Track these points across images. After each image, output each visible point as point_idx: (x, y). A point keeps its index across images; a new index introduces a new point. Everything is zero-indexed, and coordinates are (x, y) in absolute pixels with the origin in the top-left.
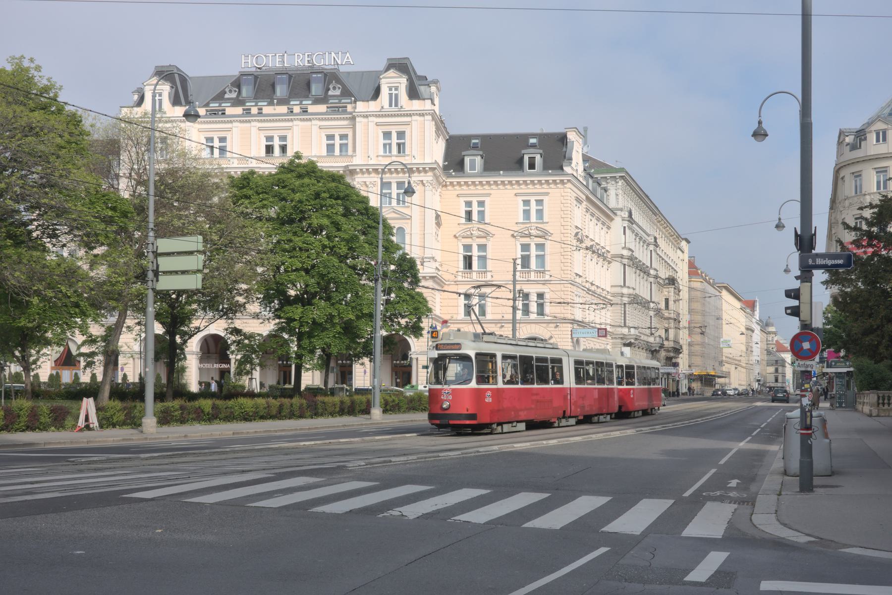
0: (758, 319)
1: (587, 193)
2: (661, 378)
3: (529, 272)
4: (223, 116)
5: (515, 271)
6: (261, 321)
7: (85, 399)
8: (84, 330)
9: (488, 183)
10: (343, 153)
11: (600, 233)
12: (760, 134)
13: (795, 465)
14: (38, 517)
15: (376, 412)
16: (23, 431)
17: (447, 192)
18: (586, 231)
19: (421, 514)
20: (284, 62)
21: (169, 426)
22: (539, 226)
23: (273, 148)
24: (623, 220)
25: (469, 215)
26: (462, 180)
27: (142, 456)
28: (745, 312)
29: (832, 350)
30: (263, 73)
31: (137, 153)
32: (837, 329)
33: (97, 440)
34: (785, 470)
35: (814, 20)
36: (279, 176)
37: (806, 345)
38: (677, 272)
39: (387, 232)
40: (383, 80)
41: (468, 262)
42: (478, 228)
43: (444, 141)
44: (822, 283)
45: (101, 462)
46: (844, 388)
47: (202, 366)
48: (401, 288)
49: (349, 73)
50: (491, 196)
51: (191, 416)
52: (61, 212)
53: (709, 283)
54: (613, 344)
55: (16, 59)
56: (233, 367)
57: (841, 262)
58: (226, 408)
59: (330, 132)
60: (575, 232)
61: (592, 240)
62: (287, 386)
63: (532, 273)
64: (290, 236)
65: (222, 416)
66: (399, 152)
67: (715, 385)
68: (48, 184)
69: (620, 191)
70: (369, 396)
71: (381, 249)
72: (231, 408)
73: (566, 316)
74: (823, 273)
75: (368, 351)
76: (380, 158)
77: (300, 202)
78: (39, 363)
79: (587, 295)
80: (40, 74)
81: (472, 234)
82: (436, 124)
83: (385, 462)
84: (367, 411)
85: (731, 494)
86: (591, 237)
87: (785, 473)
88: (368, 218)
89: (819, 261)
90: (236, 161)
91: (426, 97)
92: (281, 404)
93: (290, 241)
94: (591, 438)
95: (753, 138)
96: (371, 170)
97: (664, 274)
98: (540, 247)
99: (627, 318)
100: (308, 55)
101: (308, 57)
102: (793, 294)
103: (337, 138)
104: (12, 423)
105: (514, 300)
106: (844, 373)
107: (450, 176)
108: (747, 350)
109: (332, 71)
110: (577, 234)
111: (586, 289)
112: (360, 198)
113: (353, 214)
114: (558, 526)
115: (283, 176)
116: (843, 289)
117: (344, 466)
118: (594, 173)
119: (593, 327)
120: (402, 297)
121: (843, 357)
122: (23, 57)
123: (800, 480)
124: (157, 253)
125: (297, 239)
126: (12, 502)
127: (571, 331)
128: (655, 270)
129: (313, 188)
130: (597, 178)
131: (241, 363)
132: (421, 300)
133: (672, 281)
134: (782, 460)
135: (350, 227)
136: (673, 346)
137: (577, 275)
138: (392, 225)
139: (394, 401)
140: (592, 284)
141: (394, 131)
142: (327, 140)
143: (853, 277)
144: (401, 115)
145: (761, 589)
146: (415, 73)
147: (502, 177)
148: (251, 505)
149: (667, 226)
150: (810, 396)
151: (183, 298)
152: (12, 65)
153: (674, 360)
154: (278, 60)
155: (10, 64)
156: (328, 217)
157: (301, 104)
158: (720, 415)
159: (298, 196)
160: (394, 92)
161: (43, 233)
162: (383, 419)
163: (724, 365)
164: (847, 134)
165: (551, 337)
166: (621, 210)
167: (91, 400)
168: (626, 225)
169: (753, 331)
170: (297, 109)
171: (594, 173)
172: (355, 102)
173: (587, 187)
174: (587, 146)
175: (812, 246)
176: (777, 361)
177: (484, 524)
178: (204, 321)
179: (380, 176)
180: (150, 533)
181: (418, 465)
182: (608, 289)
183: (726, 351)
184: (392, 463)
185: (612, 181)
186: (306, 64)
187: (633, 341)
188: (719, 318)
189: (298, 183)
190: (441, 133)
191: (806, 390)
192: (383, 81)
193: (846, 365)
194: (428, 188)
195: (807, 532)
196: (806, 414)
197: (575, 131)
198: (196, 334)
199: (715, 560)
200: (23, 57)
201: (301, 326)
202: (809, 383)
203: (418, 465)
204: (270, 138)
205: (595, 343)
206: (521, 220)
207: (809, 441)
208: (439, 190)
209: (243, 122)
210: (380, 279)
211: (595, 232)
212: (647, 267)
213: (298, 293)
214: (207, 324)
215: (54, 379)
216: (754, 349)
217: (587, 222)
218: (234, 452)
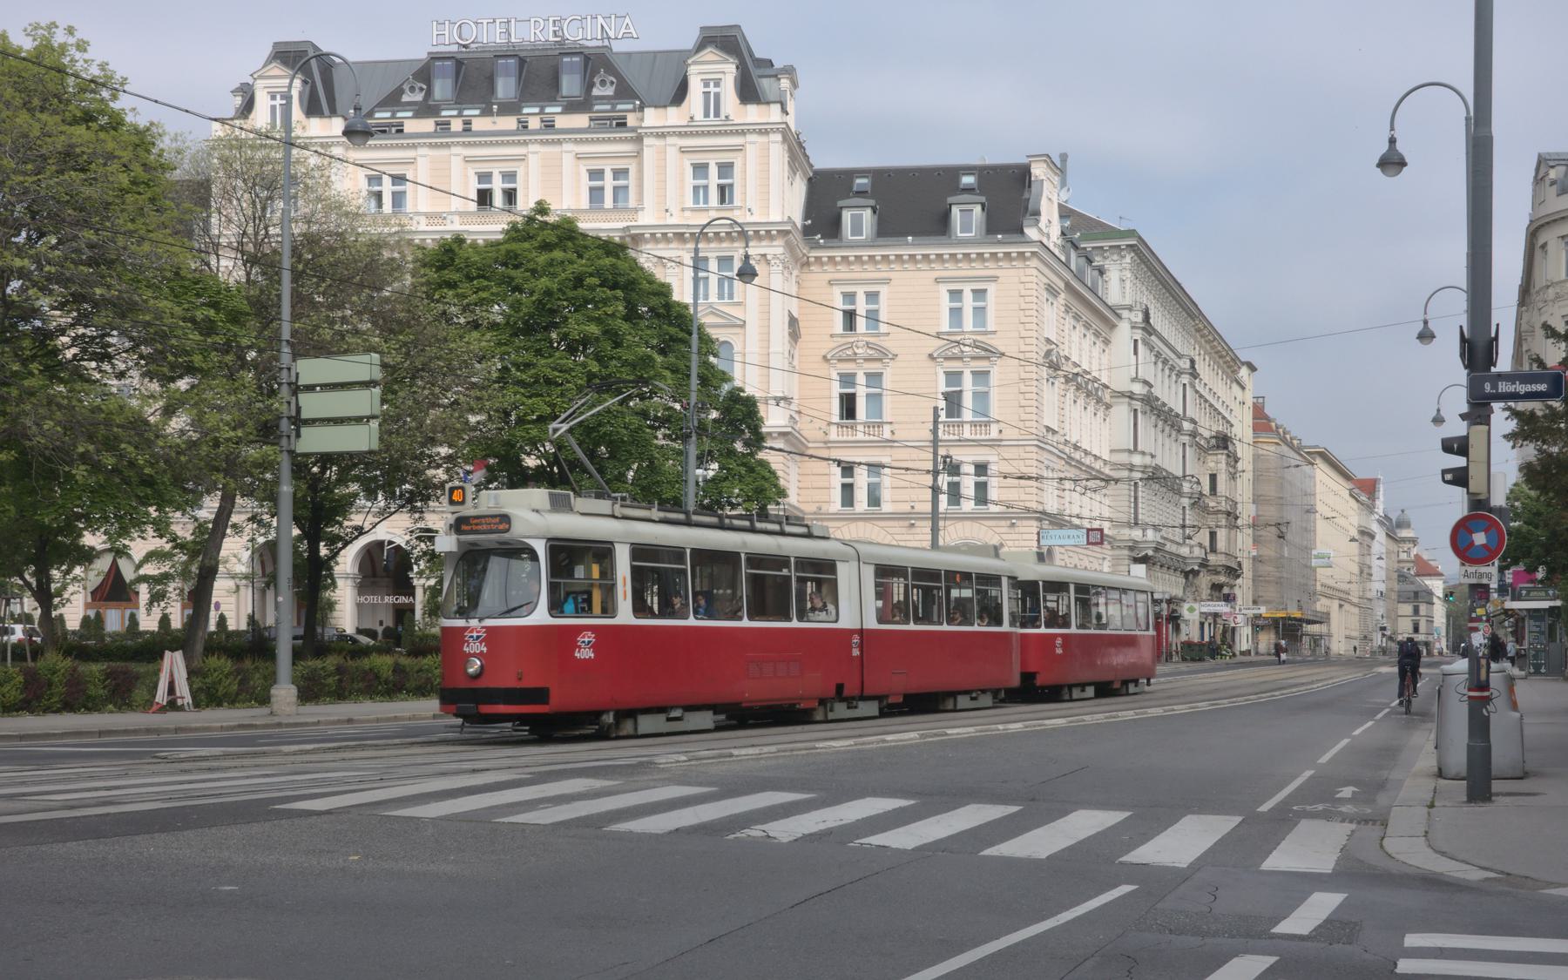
0: (1382, 514)
1: (1068, 277)
4: (399, 135)
5: (936, 422)
7: (168, 654)
8: (162, 529)
9: (885, 258)
10: (620, 205)
12: (1392, 162)
13: (1458, 759)
14: (137, 838)
16: (58, 711)
18: (1066, 347)
20: (510, 35)
21: (317, 704)
22: (979, 338)
23: (491, 194)
24: (1133, 328)
26: (838, 254)
27: (286, 748)
28: (1358, 501)
29: (1521, 567)
30: (471, 56)
31: (254, 202)
32: (1530, 527)
34: (1440, 769)
36: (507, 246)
37: (1480, 538)
38: (1232, 426)
39: (704, 350)
41: (848, 406)
42: (867, 343)
45: (216, 758)
46: (1543, 639)
47: (362, 599)
48: (731, 453)
49: (629, 54)
52: (124, 309)
53: (1291, 446)
54: (1115, 559)
55: (42, 28)
58: (418, 672)
59: (596, 165)
60: (1045, 349)
61: (1076, 365)
63: (967, 427)
64: (527, 356)
65: (411, 684)
66: (722, 200)
67: (1301, 637)
69: (1129, 275)
71: (694, 382)
72: (427, 670)
73: (1028, 505)
74: (1507, 419)
76: (687, 214)
77: (548, 293)
78: (66, 596)
79: (1067, 467)
80: (86, 56)
81: (856, 354)
82: (791, 150)
83: (720, 756)
85: (1343, 809)
86: (1074, 358)
87: (1440, 774)
88: (671, 324)
89: (1504, 387)
90: (423, 220)
91: (772, 99)
93: (528, 365)
94: (1084, 721)
95: (1407, 161)
96: (670, 235)
97: (1208, 428)
98: (980, 376)
99: (1140, 511)
100: (554, 21)
101: (554, 26)
103: (608, 175)
104: (38, 698)
105: (936, 473)
106: (1544, 610)
108: (1362, 572)
109: (598, 51)
110: (1048, 353)
111: (1065, 457)
112: (655, 286)
115: (514, 246)
117: (651, 763)
119: (1077, 527)
120: (732, 469)
121: (1541, 582)
122: (54, 25)
124: (298, 387)
125: (543, 361)
127: (1038, 534)
128: (1193, 421)
129: (570, 268)
130: (1085, 248)
132: (767, 475)
133: (1223, 442)
134: (1435, 751)
136: (1224, 563)
137: (1048, 429)
138: (714, 337)
140: (1076, 447)
141: (712, 162)
143: (1562, 425)
144: (726, 133)
145: (1406, 945)
146: (751, 54)
147: (910, 247)
148: (506, 820)
149: (1215, 339)
150: (1486, 629)
151: (332, 473)
152: (35, 40)
153: (1226, 590)
154: (498, 31)
155: (31, 38)
156: (598, 320)
157: (542, 112)
158: (1315, 686)
159: (544, 282)
160: (712, 89)
161: (84, 350)
163: (1318, 600)
164: (1552, 163)
166: (1130, 309)
167: (178, 656)
168: (1138, 337)
169: (1372, 537)
170: (534, 123)
171: (1080, 239)
172: (641, 109)
173: (1067, 265)
174: (1066, 189)
175: (1491, 360)
176: (1416, 594)
178: (370, 516)
180: (340, 860)
182: (1106, 457)
183: (1323, 575)
184: (734, 758)
185: (1113, 254)
187: (1150, 553)
188: (1311, 510)
189: (542, 259)
191: (1479, 619)
192: (693, 70)
193: (1548, 595)
194: (775, 268)
195: (1484, 864)
196: (1479, 662)
197: (1045, 161)
198: (356, 538)
199: (1319, 907)
200: (54, 25)
202: (1484, 606)
204: (484, 177)
205: (1081, 557)
206: (945, 327)
207: (1484, 710)
209: (436, 146)
210: (694, 435)
211: (1081, 350)
212: (1177, 415)
213: (545, 463)
215: (92, 625)
216: (1375, 571)
217: (1067, 331)
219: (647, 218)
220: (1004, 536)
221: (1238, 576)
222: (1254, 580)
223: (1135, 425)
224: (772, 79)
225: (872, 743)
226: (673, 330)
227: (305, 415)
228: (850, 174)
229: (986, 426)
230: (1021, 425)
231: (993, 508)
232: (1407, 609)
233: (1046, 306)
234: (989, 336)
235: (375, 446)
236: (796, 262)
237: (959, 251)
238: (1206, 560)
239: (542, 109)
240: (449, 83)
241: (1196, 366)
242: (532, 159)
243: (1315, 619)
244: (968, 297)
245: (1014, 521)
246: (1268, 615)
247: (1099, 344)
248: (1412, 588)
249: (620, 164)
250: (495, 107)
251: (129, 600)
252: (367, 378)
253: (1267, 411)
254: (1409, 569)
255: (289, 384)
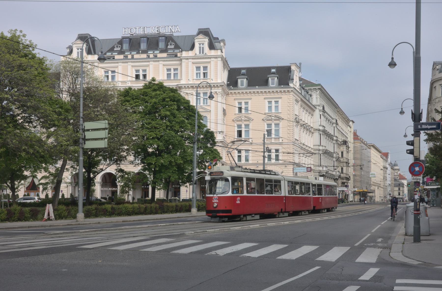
0: (390, 162)
1: (302, 97)
2: (339, 194)
3: (271, 138)
5: (264, 138)
6: (134, 165)
7: (48, 205)
10: (176, 78)
11: (308, 118)
12: (392, 64)
13: (411, 230)
15: (194, 210)
16: (17, 221)
17: (229, 98)
19: (226, 254)
20: (145, 31)
24: (320, 111)
25: (240, 109)
26: (237, 91)
28: (383, 159)
29: (429, 177)
32: (431, 166)
33: (55, 225)
35: (422, 5)
36: (144, 90)
37: (417, 169)
38: (347, 138)
40: (196, 40)
42: (245, 116)
43: (228, 71)
44: (424, 140)
46: (435, 197)
47: (103, 189)
48: (207, 147)
49: (178, 36)
50: (252, 99)
51: (101, 213)
52: (36, 109)
53: (364, 144)
55: (13, 31)
56: (119, 188)
57: (435, 127)
58: (118, 209)
59: (169, 67)
60: (295, 117)
62: (147, 198)
63: (273, 139)
64: (149, 121)
66: (204, 77)
68: (29, 95)
69: (318, 96)
70: (190, 203)
71: (196, 127)
72: (121, 209)
73: (290, 161)
74: (425, 135)
75: (189, 179)
76: (194, 81)
77: (155, 103)
78: (19, 189)
79: (301, 150)
80: (25, 38)
81: (242, 119)
84: (189, 210)
86: (303, 120)
87: (406, 235)
89: (424, 127)
90: (120, 83)
91: (218, 48)
92: (146, 207)
93: (150, 123)
94: (306, 221)
97: (341, 139)
99: (322, 162)
100: (157, 27)
102: (410, 143)
103: (172, 70)
105: (264, 152)
106: (435, 188)
107: (231, 89)
108: (384, 178)
109: (169, 36)
110: (296, 118)
111: (301, 147)
112: (185, 101)
113: (181, 109)
114: (294, 258)
115: (146, 90)
116: (435, 143)
118: (305, 86)
119: (304, 167)
120: (207, 152)
121: (434, 181)
123: (414, 237)
126: (24, 250)
127: (293, 169)
128: (337, 137)
130: (306, 89)
131: (123, 187)
132: (217, 153)
135: (181, 116)
136: (345, 176)
137: (296, 139)
138: (202, 115)
139: (202, 205)
140: (304, 145)
142: (167, 71)
143: (440, 137)
145: (396, 283)
147: (257, 89)
148: (142, 250)
149: (343, 114)
153: (346, 184)
154: (141, 30)
155: (10, 34)
156: (169, 111)
159: (154, 100)
160: (201, 46)
161: (24, 120)
162: (197, 214)
163: (372, 186)
164: (437, 64)
165: (282, 172)
166: (319, 106)
168: (321, 114)
169: (387, 169)
170: (151, 56)
171: (305, 87)
172: (182, 51)
173: (301, 94)
174: (301, 73)
175: (420, 119)
176: (399, 184)
177: (257, 257)
178: (105, 166)
179: (195, 89)
181: (220, 233)
182: (312, 147)
183: (373, 179)
184: (207, 232)
186: (156, 32)
187: (325, 174)
188: (370, 161)
189: (154, 93)
190: (226, 66)
191: (417, 191)
192: (196, 41)
193: (436, 184)
194: (219, 95)
196: (417, 203)
197: (295, 65)
200: (16, 30)
201: (156, 167)
202: (418, 188)
203: (220, 233)
204: (137, 71)
206: (267, 111)
207: (418, 217)
208: (225, 97)
209: (124, 62)
210: (196, 142)
211: (305, 118)
212: (332, 135)
214: (107, 167)
216: (388, 178)
217: (301, 112)
218: (126, 229)
219: (183, 82)
220: (283, 170)
221: (349, 180)
222: (353, 181)
223: (320, 138)
224: (218, 43)
225: (246, 228)
226: (190, 113)
227: (86, 138)
228: (240, 69)
229: (278, 139)
230: (288, 138)
231: (280, 162)
232: (397, 189)
233: (295, 105)
234: (279, 114)
235: (106, 146)
236: (225, 94)
237: (271, 90)
238: (340, 175)
239: (154, 52)
240: (128, 45)
241: (338, 122)
242: (151, 66)
243: (371, 192)
244: (273, 103)
245: (286, 165)
246: (358, 191)
247: (310, 116)
248: (398, 183)
249: (175, 67)
250: (140, 51)
251: (37, 190)
252: (104, 127)
253: (358, 134)
254: (397, 178)
255: (82, 129)
